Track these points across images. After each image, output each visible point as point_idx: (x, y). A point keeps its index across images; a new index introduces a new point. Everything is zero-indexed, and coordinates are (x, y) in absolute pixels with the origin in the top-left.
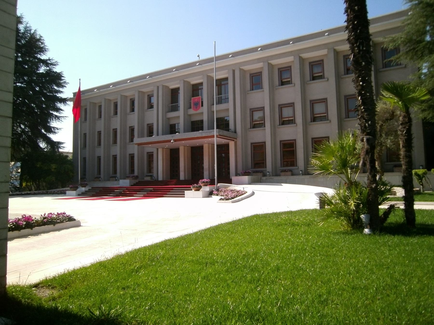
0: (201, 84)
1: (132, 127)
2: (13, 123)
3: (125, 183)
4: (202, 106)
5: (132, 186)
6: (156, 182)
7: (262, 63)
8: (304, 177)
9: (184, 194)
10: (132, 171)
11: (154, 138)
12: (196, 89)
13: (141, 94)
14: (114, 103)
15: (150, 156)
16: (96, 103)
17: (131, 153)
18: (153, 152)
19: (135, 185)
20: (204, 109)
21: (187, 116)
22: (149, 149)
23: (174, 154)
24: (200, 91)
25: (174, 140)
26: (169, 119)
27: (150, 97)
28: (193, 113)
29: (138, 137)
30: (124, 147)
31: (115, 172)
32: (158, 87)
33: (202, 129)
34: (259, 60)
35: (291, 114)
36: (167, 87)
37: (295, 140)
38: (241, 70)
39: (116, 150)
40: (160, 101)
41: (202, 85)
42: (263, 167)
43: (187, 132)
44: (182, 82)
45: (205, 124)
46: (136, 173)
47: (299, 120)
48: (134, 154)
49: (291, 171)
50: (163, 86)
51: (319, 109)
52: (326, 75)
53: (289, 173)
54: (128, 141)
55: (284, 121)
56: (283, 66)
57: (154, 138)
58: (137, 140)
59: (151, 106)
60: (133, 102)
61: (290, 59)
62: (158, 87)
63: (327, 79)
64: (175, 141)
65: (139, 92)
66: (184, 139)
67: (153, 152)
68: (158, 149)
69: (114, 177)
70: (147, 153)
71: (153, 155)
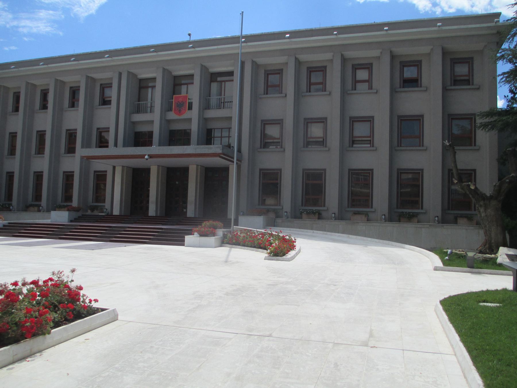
0: (154, 79)
1: (69, 130)
2: (508, 73)
3: (61, 217)
4: (190, 108)
5: (71, 221)
6: (110, 218)
7: (286, 57)
8: (337, 222)
9: (184, 241)
10: (68, 198)
11: (111, 151)
12: (176, 83)
13: (91, 81)
14: (15, 93)
15: (100, 178)
16: (9, 88)
17: (9, 171)
18: (106, 171)
19: (76, 220)
20: (194, 114)
21: (166, 122)
22: (99, 166)
23: (138, 179)
24: (150, 90)
25: (149, 155)
26: (134, 123)
27: (105, 86)
28: (174, 118)
29: (82, 147)
30: (55, 161)
31: (38, 197)
32: (120, 74)
33: (187, 142)
34: (283, 52)
35: (367, 133)
36: (135, 75)
37: (325, 170)
38: (254, 64)
39: (42, 164)
40: (120, 95)
41: (233, 75)
42: (367, 206)
43: (163, 146)
44: (161, 70)
45: (194, 137)
46: (75, 203)
47: (288, 145)
48: (13, 173)
49: (366, 214)
50: (129, 73)
51: (361, 130)
52: (425, 81)
53: (364, 217)
54: (63, 150)
55: (266, 143)
56: (314, 65)
57: (111, 151)
58: (81, 152)
59: (105, 102)
60: (45, 94)
61: (328, 56)
62: (120, 74)
63: (329, 93)
64: (151, 156)
65: (88, 77)
66: (156, 156)
67: (106, 171)
68: (114, 168)
69: (34, 204)
70: (95, 172)
71: (42, 176)
